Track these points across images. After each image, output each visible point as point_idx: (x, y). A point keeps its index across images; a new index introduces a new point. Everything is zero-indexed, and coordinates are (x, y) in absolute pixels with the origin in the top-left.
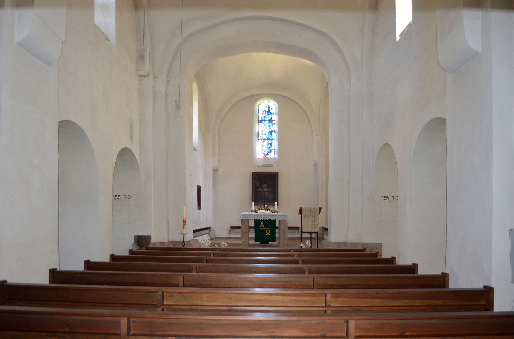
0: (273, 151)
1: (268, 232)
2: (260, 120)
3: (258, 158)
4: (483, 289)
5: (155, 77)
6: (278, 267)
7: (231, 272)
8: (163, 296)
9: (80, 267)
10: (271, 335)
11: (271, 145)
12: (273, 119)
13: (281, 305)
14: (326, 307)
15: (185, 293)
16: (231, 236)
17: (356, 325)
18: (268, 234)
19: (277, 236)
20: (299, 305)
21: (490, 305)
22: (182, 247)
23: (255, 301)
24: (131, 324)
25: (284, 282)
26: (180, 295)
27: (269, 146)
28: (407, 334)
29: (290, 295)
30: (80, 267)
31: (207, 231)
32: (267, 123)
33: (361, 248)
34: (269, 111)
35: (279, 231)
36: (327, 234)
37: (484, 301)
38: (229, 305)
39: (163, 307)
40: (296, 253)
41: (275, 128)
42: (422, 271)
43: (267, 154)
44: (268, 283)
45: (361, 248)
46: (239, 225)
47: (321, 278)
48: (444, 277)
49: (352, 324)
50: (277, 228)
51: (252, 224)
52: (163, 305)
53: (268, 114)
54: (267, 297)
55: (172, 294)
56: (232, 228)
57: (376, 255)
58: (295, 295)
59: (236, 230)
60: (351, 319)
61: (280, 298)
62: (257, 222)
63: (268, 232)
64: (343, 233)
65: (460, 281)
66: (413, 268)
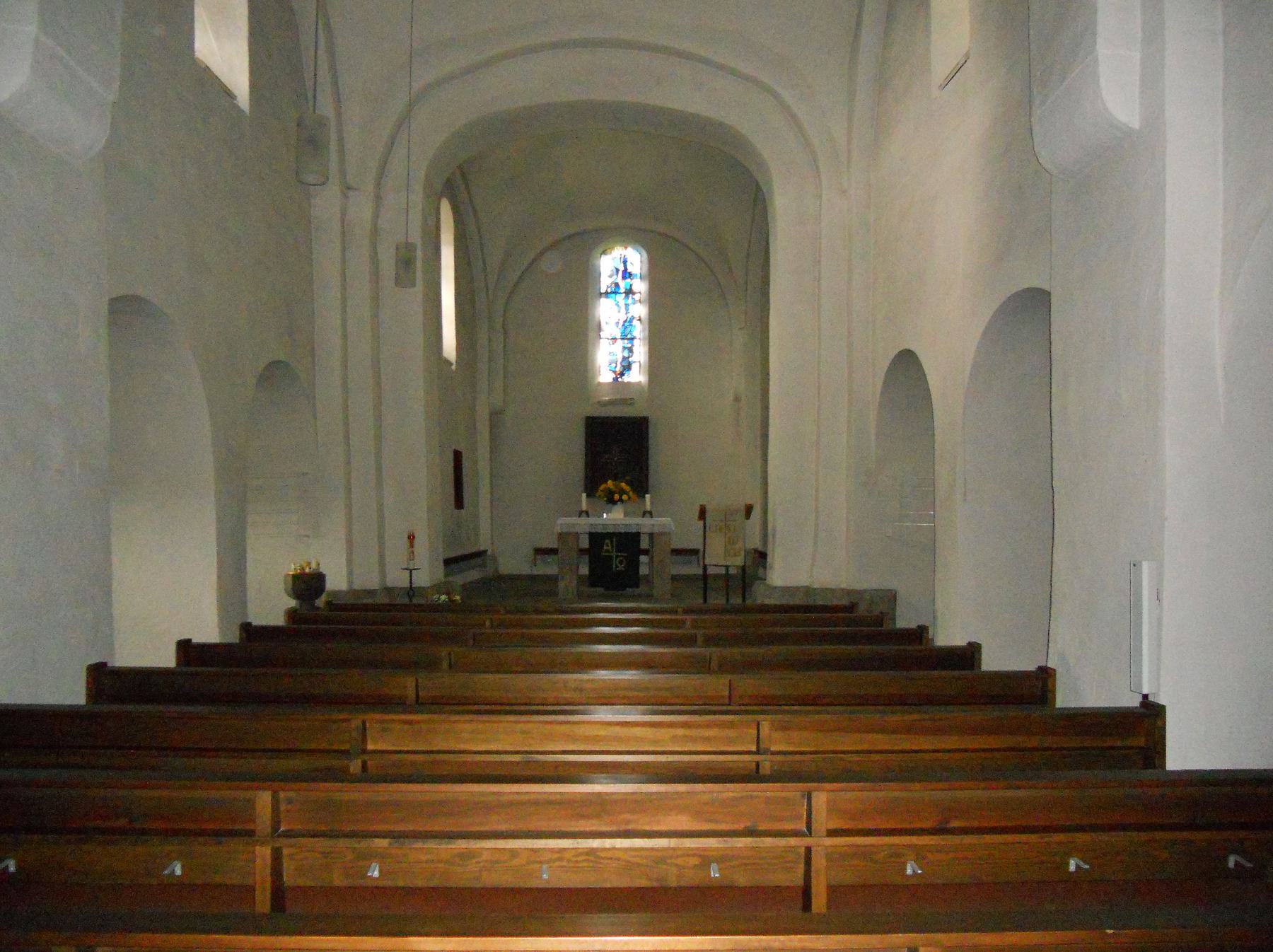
0: (635, 367)
1: (621, 562)
2: (603, 290)
3: (600, 384)
4: (1142, 710)
5: (349, 188)
6: (644, 654)
7: (410, 779)
8: (365, 729)
9: (167, 659)
10: (623, 828)
11: (630, 350)
12: (634, 289)
13: (651, 749)
14: (758, 752)
15: (418, 722)
16: (536, 572)
17: (828, 802)
18: (621, 567)
19: (644, 570)
20: (694, 749)
21: (1155, 750)
22: (406, 601)
23: (587, 739)
24: (283, 807)
25: (661, 689)
26: (406, 727)
27: (626, 354)
28: (955, 824)
29: (671, 725)
30: (167, 659)
31: (479, 561)
32: (620, 298)
33: (845, 602)
34: (626, 269)
35: (651, 559)
36: (765, 567)
37: (1143, 739)
38: (526, 749)
39: (366, 757)
40: (689, 618)
41: (640, 310)
42: (991, 662)
43: (622, 374)
44: (622, 693)
45: (845, 602)
46: (552, 543)
47: (748, 684)
48: (1045, 676)
49: (821, 799)
50: (646, 552)
51: (585, 543)
52: (364, 751)
53: (624, 278)
54: (617, 729)
55: (385, 725)
56: (540, 552)
57: (879, 620)
58: (685, 725)
59: (550, 559)
60: (817, 790)
61: (647, 732)
62: (597, 538)
63: (621, 562)
64: (806, 563)
65: (1087, 687)
66: (969, 655)
